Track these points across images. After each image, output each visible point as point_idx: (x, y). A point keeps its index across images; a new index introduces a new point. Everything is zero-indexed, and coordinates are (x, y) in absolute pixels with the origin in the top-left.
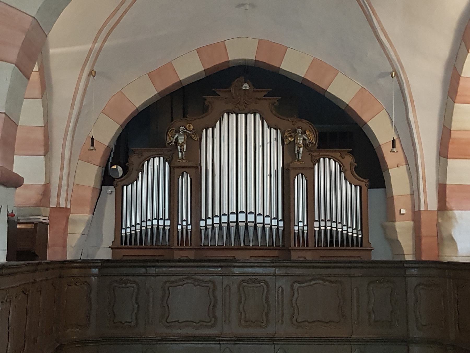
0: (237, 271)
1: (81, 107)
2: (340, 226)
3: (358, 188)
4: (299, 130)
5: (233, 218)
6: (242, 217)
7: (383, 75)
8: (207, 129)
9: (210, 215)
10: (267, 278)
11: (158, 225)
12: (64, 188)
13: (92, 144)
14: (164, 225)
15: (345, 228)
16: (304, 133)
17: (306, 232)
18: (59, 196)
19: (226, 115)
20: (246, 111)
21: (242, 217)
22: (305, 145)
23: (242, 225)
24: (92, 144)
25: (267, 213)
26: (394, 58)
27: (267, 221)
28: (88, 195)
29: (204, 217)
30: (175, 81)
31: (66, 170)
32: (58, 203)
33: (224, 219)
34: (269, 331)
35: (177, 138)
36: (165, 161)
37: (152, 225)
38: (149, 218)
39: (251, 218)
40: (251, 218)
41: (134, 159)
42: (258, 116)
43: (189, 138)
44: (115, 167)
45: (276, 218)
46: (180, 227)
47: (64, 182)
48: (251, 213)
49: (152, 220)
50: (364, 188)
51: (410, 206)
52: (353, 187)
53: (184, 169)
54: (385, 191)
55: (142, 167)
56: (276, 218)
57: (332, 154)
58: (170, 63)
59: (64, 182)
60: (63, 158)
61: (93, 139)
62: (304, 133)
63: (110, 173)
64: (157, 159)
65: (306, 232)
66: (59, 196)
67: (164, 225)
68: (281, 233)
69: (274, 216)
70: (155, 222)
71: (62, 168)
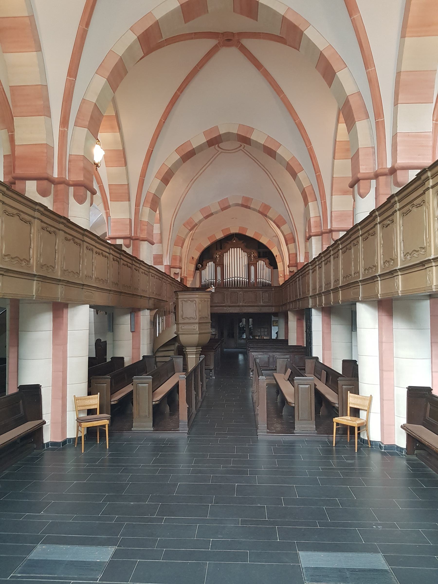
0: (230, 290)
1: (189, 249)
2: (265, 280)
3: (270, 269)
4: (252, 253)
5: (233, 279)
6: (236, 279)
7: (274, 237)
8: (225, 253)
9: (227, 278)
10: (237, 292)
11: (212, 281)
12: (185, 271)
13: (193, 259)
14: (214, 281)
15: (266, 281)
16: (253, 253)
17: (214, 282)
18: (184, 273)
19: (231, 249)
20: (237, 247)
21: (236, 279)
22: (254, 257)
23: (241, 281)
24: (193, 259)
25: (243, 277)
26: (276, 232)
27: (243, 279)
28: (192, 273)
29: (225, 279)
30: (215, 240)
31: (186, 266)
32: (184, 275)
33: (231, 279)
34: (237, 305)
35: (216, 256)
36: (213, 263)
37: (210, 281)
38: (209, 279)
39: (239, 279)
40: (239, 279)
41: (204, 262)
42: (240, 248)
43: (220, 256)
44: (199, 265)
45: (246, 278)
46: (218, 281)
47: (186, 269)
48: (239, 277)
49: (210, 280)
50: (272, 269)
51: (283, 274)
52: (269, 269)
53: (219, 265)
54: (69, 303)
55: (207, 265)
56: (246, 278)
57: (264, 260)
58: (214, 234)
59: (186, 269)
60: (185, 263)
61: (193, 257)
62: (253, 253)
63: (198, 267)
64: (211, 262)
65: (214, 282)
66: (184, 273)
67: (214, 281)
68: (247, 283)
69: (245, 278)
70: (211, 280)
71: (185, 266)
